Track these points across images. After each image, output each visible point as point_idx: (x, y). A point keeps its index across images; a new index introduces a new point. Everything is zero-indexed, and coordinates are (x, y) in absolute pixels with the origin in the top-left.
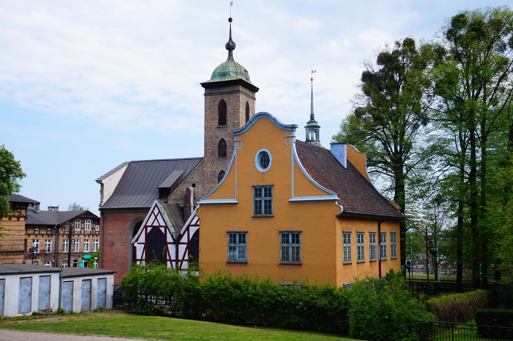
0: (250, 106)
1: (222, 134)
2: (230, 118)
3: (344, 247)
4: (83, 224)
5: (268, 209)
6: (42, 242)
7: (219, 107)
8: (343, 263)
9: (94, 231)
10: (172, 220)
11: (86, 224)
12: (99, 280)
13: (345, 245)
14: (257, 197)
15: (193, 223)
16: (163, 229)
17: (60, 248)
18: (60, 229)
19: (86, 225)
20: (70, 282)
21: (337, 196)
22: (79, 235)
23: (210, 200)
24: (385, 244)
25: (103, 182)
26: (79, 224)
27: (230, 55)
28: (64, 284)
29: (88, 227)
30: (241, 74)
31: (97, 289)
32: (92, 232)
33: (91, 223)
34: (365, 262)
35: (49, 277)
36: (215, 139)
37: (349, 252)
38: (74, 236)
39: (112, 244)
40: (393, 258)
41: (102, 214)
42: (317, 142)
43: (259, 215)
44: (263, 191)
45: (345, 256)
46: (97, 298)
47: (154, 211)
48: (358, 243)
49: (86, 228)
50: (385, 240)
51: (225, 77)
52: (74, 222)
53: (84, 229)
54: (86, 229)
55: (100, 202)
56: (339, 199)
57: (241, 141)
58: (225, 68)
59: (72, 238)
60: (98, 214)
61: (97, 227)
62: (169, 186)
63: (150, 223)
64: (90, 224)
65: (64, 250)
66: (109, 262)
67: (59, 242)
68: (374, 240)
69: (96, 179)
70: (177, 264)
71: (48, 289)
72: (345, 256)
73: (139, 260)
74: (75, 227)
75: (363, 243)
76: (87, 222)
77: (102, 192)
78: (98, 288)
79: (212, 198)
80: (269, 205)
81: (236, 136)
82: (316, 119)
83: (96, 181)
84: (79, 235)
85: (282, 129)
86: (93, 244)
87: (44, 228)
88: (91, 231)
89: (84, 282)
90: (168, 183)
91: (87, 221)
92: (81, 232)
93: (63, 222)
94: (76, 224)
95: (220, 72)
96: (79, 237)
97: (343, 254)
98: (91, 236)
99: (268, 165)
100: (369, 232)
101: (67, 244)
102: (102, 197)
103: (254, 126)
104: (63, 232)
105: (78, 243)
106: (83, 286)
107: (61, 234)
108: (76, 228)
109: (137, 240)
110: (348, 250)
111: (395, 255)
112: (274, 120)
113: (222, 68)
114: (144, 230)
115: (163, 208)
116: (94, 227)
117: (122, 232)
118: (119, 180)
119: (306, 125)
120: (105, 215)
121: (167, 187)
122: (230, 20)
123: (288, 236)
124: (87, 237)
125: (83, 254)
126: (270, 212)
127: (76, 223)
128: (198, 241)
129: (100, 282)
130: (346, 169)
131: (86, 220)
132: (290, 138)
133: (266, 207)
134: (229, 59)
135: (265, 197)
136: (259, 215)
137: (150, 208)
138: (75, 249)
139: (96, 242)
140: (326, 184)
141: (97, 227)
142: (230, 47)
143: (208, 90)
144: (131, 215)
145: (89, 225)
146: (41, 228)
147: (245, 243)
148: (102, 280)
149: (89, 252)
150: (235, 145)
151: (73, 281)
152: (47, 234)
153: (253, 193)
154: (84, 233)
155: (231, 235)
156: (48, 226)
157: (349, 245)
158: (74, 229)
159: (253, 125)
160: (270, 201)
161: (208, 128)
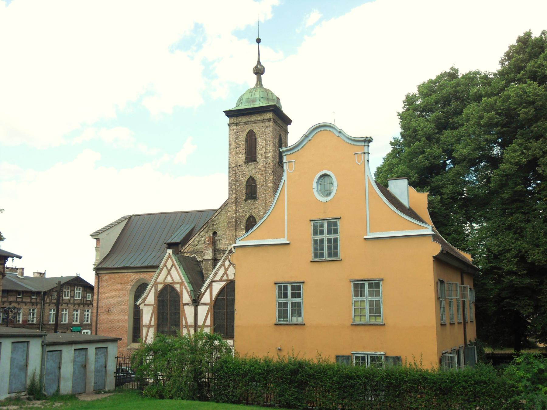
0: (283, 140)
1: (249, 170)
4: (72, 293)
6: (25, 311)
7: (246, 139)
9: (85, 300)
10: (189, 276)
12: (97, 349)
15: (218, 278)
16: (177, 287)
17: (46, 318)
18: (46, 297)
20: (56, 352)
22: (67, 304)
27: (259, 80)
28: (48, 355)
29: (78, 295)
31: (94, 362)
35: (26, 344)
36: (242, 177)
38: (62, 306)
46: (95, 374)
47: (167, 264)
49: (76, 296)
51: (254, 104)
52: (63, 289)
53: (73, 297)
59: (60, 307)
60: (90, 278)
61: (89, 295)
62: (178, 241)
63: (160, 279)
64: (81, 292)
65: (62, 321)
66: (104, 332)
67: (45, 312)
69: (91, 233)
70: (195, 331)
71: (25, 361)
73: (146, 326)
77: (97, 248)
78: (95, 361)
80: (333, 244)
83: (91, 235)
84: (67, 304)
86: (83, 315)
87: (28, 295)
88: (81, 300)
89: (77, 352)
91: (77, 289)
92: (70, 300)
93: (50, 289)
94: (65, 291)
96: (67, 306)
98: (82, 306)
101: (54, 314)
103: (312, 141)
104: (49, 300)
106: (75, 358)
107: (47, 303)
108: (65, 296)
109: (144, 301)
112: (340, 132)
114: (154, 288)
116: (85, 296)
117: (121, 296)
122: (258, 41)
123: (362, 286)
124: (77, 306)
125: (71, 325)
126: (336, 255)
129: (99, 353)
131: (76, 287)
132: (362, 154)
133: (329, 248)
135: (328, 234)
138: (62, 319)
141: (89, 295)
142: (259, 71)
143: (232, 120)
144: (132, 275)
146: (25, 294)
147: (279, 303)
148: (102, 349)
149: (79, 323)
151: (61, 351)
152: (31, 302)
154: (74, 302)
156: (31, 293)
158: (63, 297)
160: (336, 240)
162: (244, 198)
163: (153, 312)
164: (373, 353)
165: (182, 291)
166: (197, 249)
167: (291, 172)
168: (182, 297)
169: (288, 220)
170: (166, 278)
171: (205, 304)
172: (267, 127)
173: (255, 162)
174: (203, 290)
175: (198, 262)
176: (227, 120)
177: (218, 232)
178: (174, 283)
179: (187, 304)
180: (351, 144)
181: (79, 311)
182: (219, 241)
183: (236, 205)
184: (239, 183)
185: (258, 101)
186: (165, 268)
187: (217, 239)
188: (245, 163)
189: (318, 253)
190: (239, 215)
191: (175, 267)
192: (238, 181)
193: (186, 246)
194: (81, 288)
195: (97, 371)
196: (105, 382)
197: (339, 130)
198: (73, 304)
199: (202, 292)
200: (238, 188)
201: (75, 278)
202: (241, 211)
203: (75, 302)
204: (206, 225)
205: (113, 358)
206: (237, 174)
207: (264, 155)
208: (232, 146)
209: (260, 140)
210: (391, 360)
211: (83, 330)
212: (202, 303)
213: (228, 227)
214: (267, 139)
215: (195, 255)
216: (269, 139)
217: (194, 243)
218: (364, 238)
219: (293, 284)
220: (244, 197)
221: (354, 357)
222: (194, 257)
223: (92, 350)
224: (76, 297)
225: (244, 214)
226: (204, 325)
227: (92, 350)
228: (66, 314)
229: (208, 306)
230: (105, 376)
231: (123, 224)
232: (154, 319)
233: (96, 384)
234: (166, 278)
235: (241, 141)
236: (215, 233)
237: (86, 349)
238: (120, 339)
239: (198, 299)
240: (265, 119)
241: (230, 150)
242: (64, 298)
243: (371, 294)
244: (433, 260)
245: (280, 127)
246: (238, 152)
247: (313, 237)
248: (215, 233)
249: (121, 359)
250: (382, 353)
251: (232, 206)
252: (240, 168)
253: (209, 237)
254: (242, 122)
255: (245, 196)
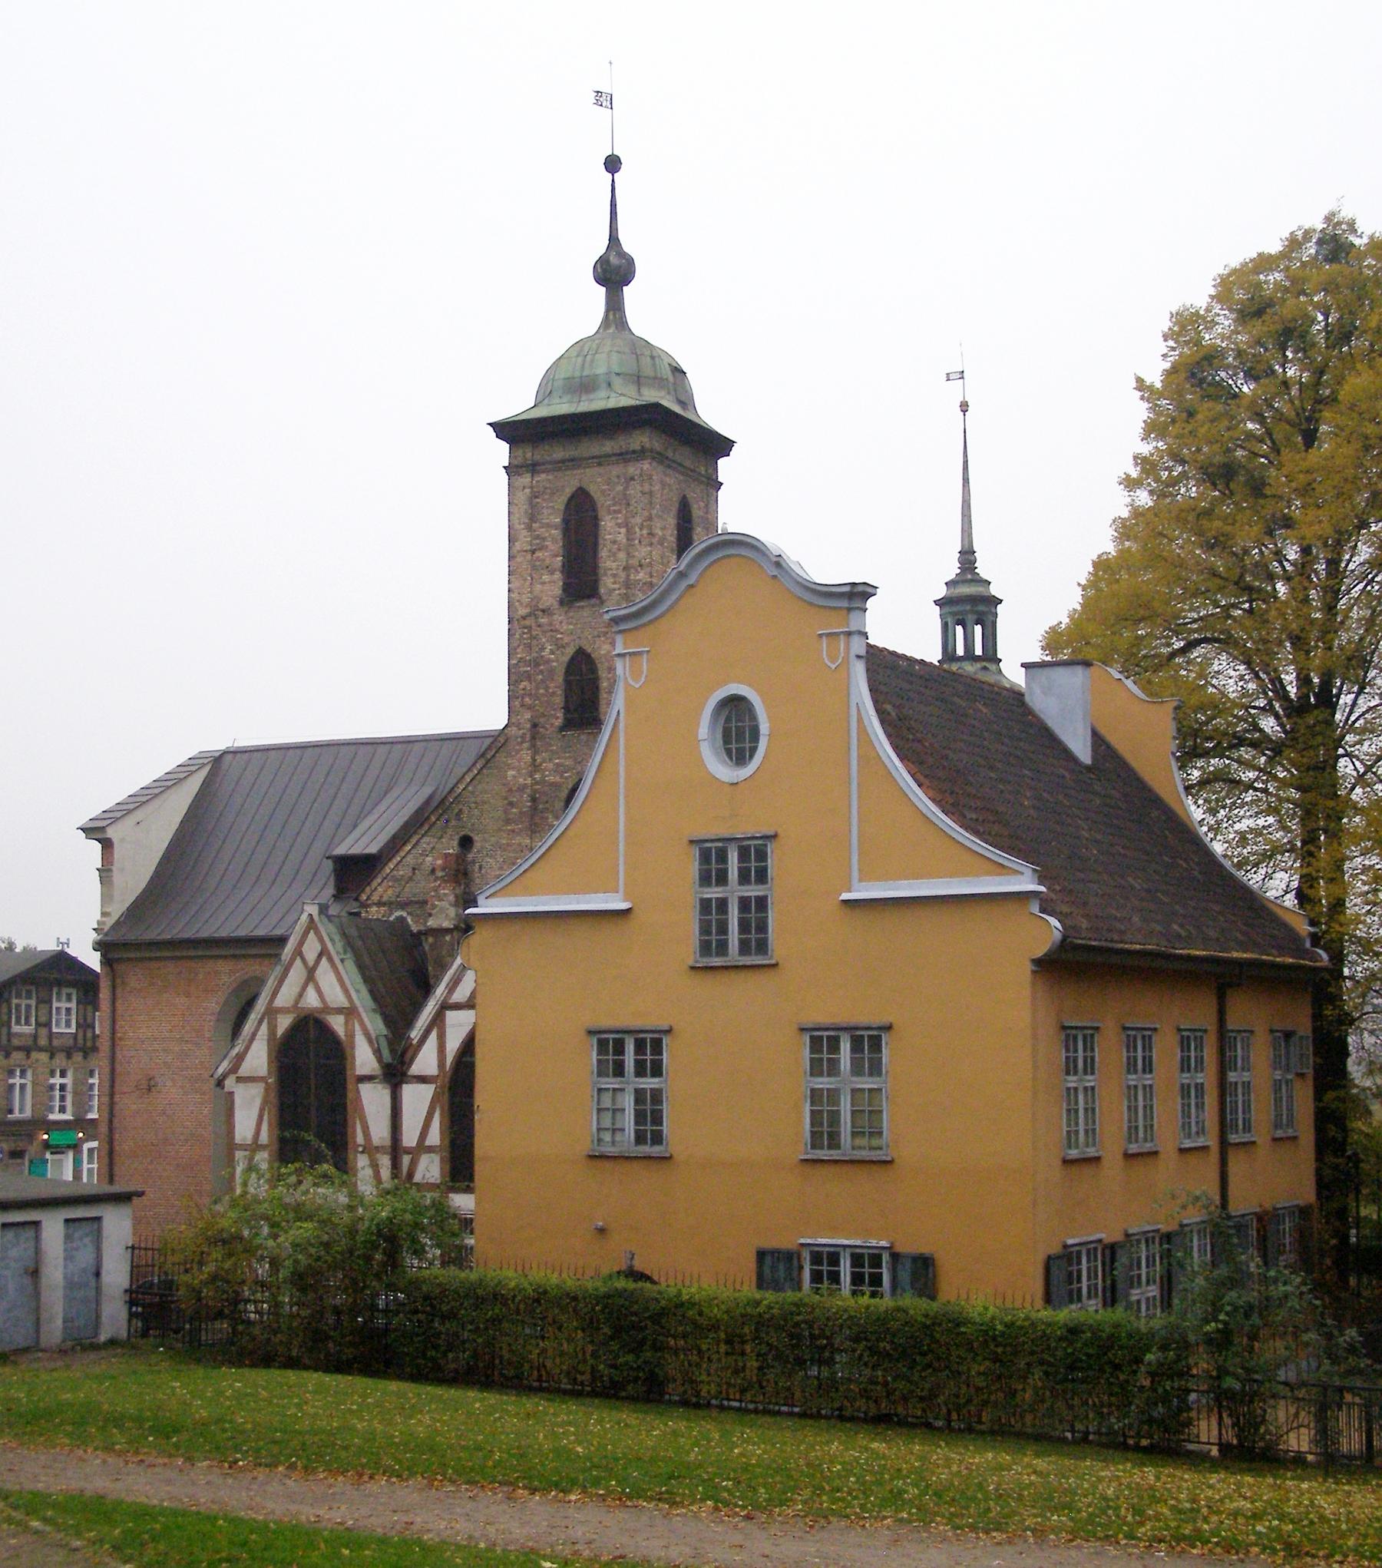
0: (697, 512)
2: (614, 565)
3: (1068, 1089)
4: (44, 1010)
5: (753, 936)
7: (566, 521)
8: (1062, 1154)
9: (89, 1035)
11: (55, 1005)
13: (1072, 1081)
14: (709, 885)
16: (337, 1023)
19: (58, 1009)
21: (1028, 873)
22: (28, 1051)
23: (521, 899)
24: (1246, 1076)
25: (111, 833)
26: (28, 1007)
27: (615, 307)
30: (658, 381)
31: (61, 1261)
32: (80, 1041)
33: (78, 1003)
34: (1156, 1153)
36: (552, 652)
37: (1090, 1111)
39: (150, 1086)
40: (1279, 1133)
41: (106, 961)
42: (987, 665)
43: (717, 961)
44: (733, 858)
45: (1069, 1125)
47: (305, 949)
48: (1129, 1072)
50: (1246, 1059)
51: (592, 396)
53: (48, 1025)
54: (57, 1025)
55: (98, 917)
56: (1042, 889)
57: (640, 653)
58: (592, 361)
60: (93, 960)
62: (373, 849)
63: (285, 998)
64: (73, 1005)
65: (11, 1111)
68: (1200, 1061)
69: (83, 820)
70: (395, 1164)
72: (1090, 1127)
74: (13, 1020)
75: (1151, 1071)
76: (59, 1000)
77: (105, 873)
78: (65, 1259)
79: (529, 892)
80: (755, 911)
81: (620, 632)
82: (983, 570)
84: (28, 1051)
85: (811, 604)
90: (365, 839)
92: (35, 1037)
94: (18, 1006)
95: (568, 375)
96: (28, 1057)
97: (1061, 1118)
98: (78, 1057)
99: (753, 751)
100: (1179, 1030)
102: (106, 897)
105: (68, 1081)
108: (18, 1022)
109: (234, 1069)
110: (1086, 1103)
111: (1291, 1122)
112: (778, 565)
113: (580, 359)
114: (264, 1027)
115: (337, 938)
116: (89, 1020)
118: (175, 826)
119: (942, 592)
120: (120, 968)
121: (367, 851)
122: (612, 164)
126: (762, 947)
127: (15, 1001)
128: (471, 1067)
129: (76, 1235)
130: (1089, 769)
131: (55, 990)
132: (842, 636)
134: (606, 323)
135: (741, 883)
136: (717, 961)
137: (282, 940)
139: (57, 1081)
140: (996, 828)
143: (520, 452)
144: (223, 966)
145: (68, 1010)
147: (660, 1075)
148: (84, 1223)
150: (619, 671)
153: (694, 868)
155: (602, 1045)
157: (1090, 1081)
158: (10, 1027)
159: (691, 586)
160: (762, 903)
161: (521, 604)
162: (558, 722)
163: (265, 1102)
164: (858, 1243)
165: (351, 1035)
166: (409, 891)
167: (637, 686)
168: (353, 1057)
169: (627, 836)
170: (301, 995)
171: (423, 1079)
172: (632, 479)
173: (593, 601)
174: (415, 1034)
175: (413, 935)
176: (501, 450)
177: (476, 838)
178: (327, 1009)
179: (369, 1078)
180: (811, 604)
181: (70, 1074)
182: (481, 867)
183: (533, 746)
184: (541, 672)
185: (604, 385)
186: (298, 961)
187: (474, 862)
188: (562, 603)
189: (712, 940)
190: (542, 782)
191: (330, 960)
192: (537, 665)
193: (375, 884)
194: (74, 992)
195: (70, 1285)
196: (98, 1317)
197: (775, 559)
198: (46, 1051)
199: (415, 1042)
200: (537, 688)
201: (53, 957)
202: (551, 766)
203: (56, 1043)
204: (437, 814)
205: (121, 1250)
206: (534, 642)
207: (623, 575)
208: (518, 546)
209: (609, 524)
210: (908, 1265)
211: (87, 1140)
212: (415, 1077)
213: (508, 821)
214: (633, 521)
215: (404, 914)
216: (638, 520)
217: (401, 873)
218: (841, 898)
219: (642, 1036)
220: (557, 718)
221: (806, 1255)
222: (402, 919)
223: (53, 1225)
224: (57, 1025)
225: (558, 779)
226: (422, 1148)
227: (53, 1225)
228: (23, 1087)
229: (433, 1086)
230: (98, 1302)
231: (194, 784)
232: (270, 1124)
233: (70, 1324)
234: (301, 995)
235: (548, 526)
236: (466, 842)
237: (36, 1224)
238: (141, 1194)
239: (403, 1063)
240: (627, 453)
241: (510, 558)
242: (16, 1029)
243: (857, 1069)
244: (1034, 972)
245: (682, 474)
246: (538, 563)
247: (697, 893)
248: (466, 842)
249: (150, 1253)
250: (883, 1243)
251: (518, 752)
252: (543, 620)
253: (447, 855)
254: (550, 463)
255: (560, 714)
